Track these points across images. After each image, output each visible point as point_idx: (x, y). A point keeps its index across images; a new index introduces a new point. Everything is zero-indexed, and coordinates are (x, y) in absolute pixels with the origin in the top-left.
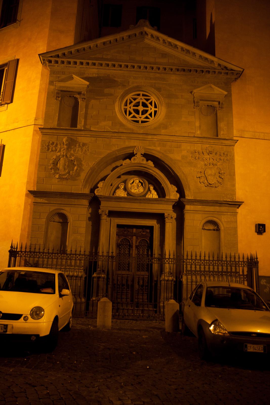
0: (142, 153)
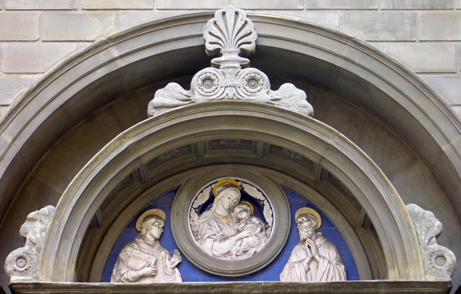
0: (244, 46)
